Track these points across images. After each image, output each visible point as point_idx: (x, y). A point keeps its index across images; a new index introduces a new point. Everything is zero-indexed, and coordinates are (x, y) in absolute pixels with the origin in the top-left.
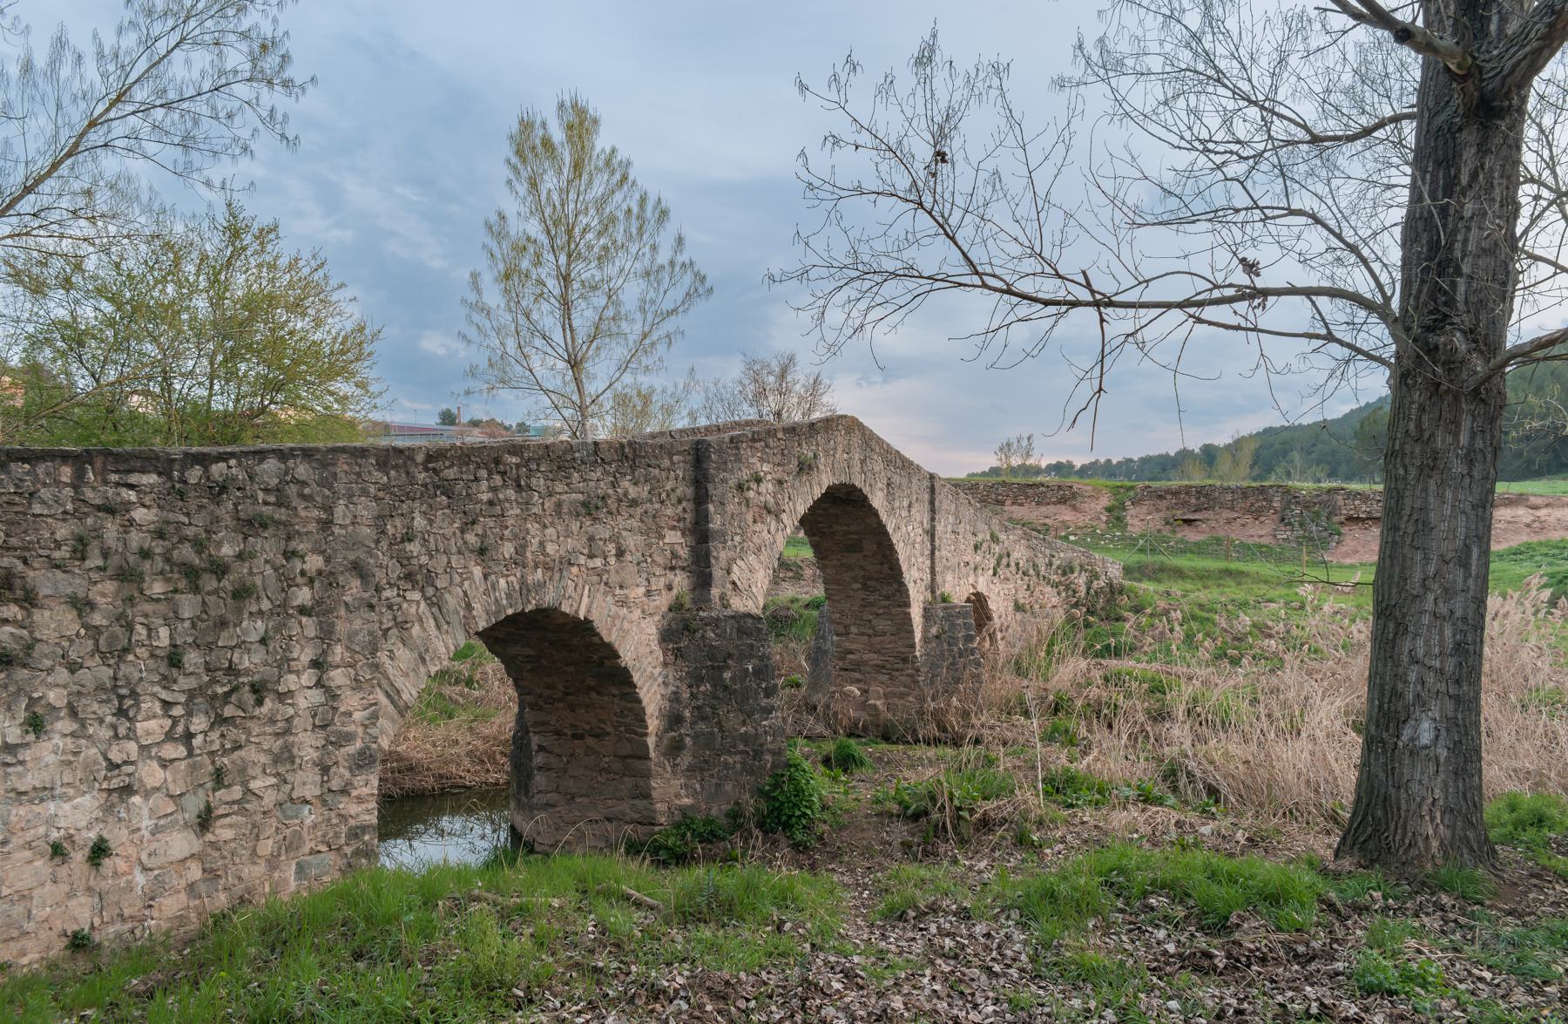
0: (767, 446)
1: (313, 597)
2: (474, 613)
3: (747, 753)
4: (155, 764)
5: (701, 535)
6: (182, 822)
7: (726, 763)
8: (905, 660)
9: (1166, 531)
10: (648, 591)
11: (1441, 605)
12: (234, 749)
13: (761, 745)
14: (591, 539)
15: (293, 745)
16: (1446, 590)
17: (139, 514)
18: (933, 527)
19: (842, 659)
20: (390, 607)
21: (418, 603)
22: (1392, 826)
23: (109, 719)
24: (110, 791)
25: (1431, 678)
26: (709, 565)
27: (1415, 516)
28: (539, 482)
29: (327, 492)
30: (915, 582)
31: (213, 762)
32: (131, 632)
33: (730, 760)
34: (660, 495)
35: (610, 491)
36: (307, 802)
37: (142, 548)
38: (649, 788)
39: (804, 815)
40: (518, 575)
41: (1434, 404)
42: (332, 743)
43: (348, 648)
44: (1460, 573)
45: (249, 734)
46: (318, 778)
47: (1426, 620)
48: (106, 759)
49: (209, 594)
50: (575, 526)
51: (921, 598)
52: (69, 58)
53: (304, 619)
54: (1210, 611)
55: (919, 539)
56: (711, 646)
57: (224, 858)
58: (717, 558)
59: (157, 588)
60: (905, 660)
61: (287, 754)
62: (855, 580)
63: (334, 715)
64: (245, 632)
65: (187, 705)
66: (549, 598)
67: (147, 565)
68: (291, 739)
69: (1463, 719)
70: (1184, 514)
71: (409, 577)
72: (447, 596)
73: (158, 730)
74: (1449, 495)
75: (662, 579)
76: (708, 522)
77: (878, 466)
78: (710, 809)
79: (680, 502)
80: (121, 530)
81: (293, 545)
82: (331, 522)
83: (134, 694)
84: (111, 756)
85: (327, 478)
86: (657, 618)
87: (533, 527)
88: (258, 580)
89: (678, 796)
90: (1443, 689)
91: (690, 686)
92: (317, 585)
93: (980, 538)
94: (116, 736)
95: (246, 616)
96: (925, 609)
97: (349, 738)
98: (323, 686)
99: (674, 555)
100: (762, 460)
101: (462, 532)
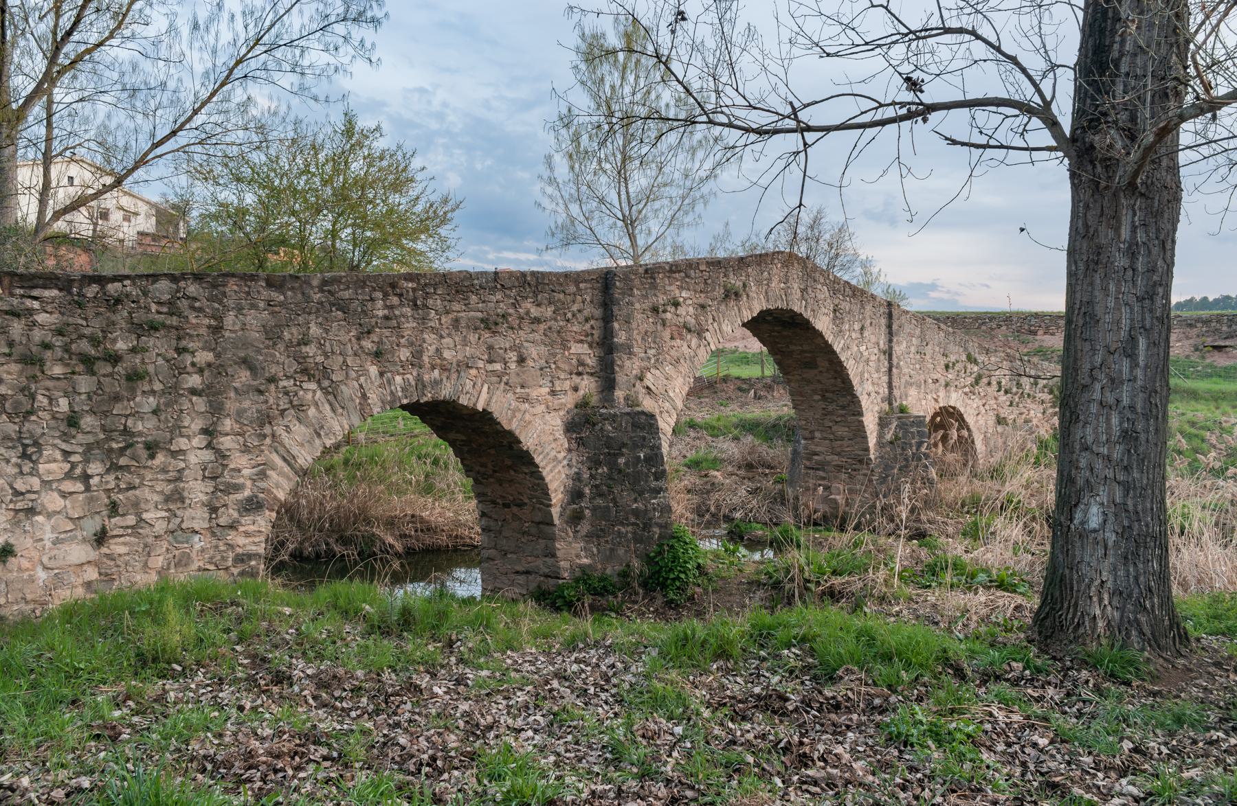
0: (687, 276)
1: (203, 382)
2: (369, 401)
3: (638, 525)
4: (55, 494)
5: (607, 348)
6: (80, 538)
7: (619, 532)
8: (861, 462)
9: (1195, 357)
10: (552, 391)
11: (1108, 394)
12: (128, 489)
13: (650, 519)
14: (490, 348)
15: (183, 489)
16: (1112, 380)
17: (41, 318)
18: (891, 348)
19: (809, 459)
20: (287, 393)
21: (314, 391)
22: (1066, 605)
23: (14, 460)
24: (17, 511)
25: (1099, 465)
26: (613, 372)
27: (1083, 310)
28: (436, 302)
29: (216, 305)
30: (869, 395)
31: (109, 497)
32: (34, 400)
33: (623, 530)
34: (565, 314)
35: (511, 311)
36: (197, 532)
37: (43, 342)
38: (555, 548)
39: (678, 578)
40: (415, 373)
41: (1095, 201)
42: (221, 491)
43: (237, 421)
44: (1126, 364)
45: (143, 479)
46: (207, 515)
47: (1094, 408)
48: (12, 488)
49: (104, 376)
50: (473, 337)
51: (877, 408)
52: (225, 16)
53: (194, 398)
54: (1202, 428)
55: (873, 358)
56: (608, 437)
57: (118, 566)
58: (621, 367)
59: (58, 370)
60: (861, 462)
61: (177, 496)
62: (815, 392)
63: (223, 470)
64: (138, 405)
65: (85, 455)
66: (446, 392)
67: (48, 354)
68: (182, 485)
69: (1135, 506)
70: (1215, 341)
71: (305, 371)
72: (343, 387)
73: (59, 471)
74: (1112, 287)
75: (568, 382)
76: (613, 337)
77: (823, 292)
78: (605, 569)
79: (587, 320)
80: (26, 328)
81: (184, 343)
82: (222, 328)
83: (36, 444)
84: (16, 486)
85: (216, 295)
86: (562, 413)
87: (429, 337)
88: (151, 368)
89: (578, 556)
90: (1111, 475)
91: (590, 469)
92: (206, 373)
93: (953, 358)
94: (21, 473)
95: (139, 393)
96: (880, 418)
97: (238, 488)
98: (214, 448)
99: (581, 363)
100: (681, 288)
101: (358, 339)
